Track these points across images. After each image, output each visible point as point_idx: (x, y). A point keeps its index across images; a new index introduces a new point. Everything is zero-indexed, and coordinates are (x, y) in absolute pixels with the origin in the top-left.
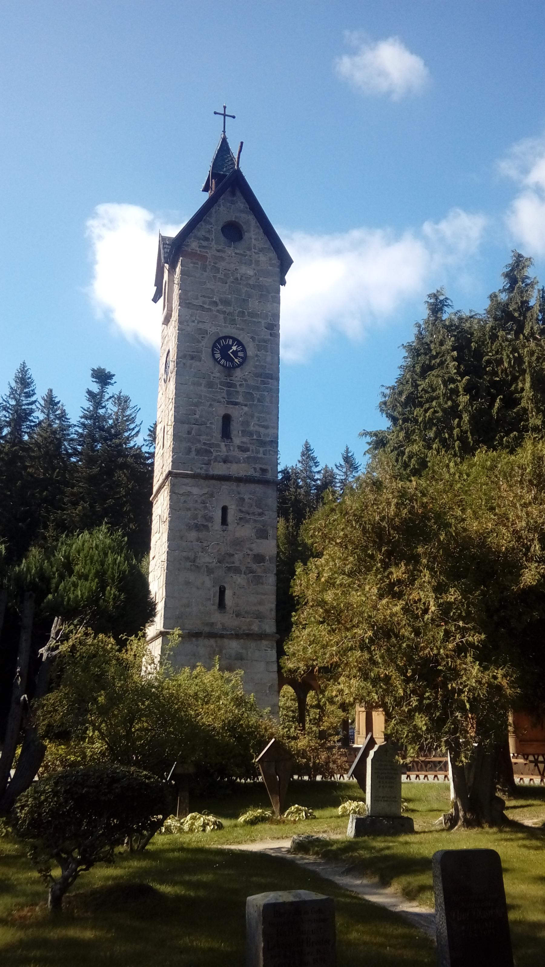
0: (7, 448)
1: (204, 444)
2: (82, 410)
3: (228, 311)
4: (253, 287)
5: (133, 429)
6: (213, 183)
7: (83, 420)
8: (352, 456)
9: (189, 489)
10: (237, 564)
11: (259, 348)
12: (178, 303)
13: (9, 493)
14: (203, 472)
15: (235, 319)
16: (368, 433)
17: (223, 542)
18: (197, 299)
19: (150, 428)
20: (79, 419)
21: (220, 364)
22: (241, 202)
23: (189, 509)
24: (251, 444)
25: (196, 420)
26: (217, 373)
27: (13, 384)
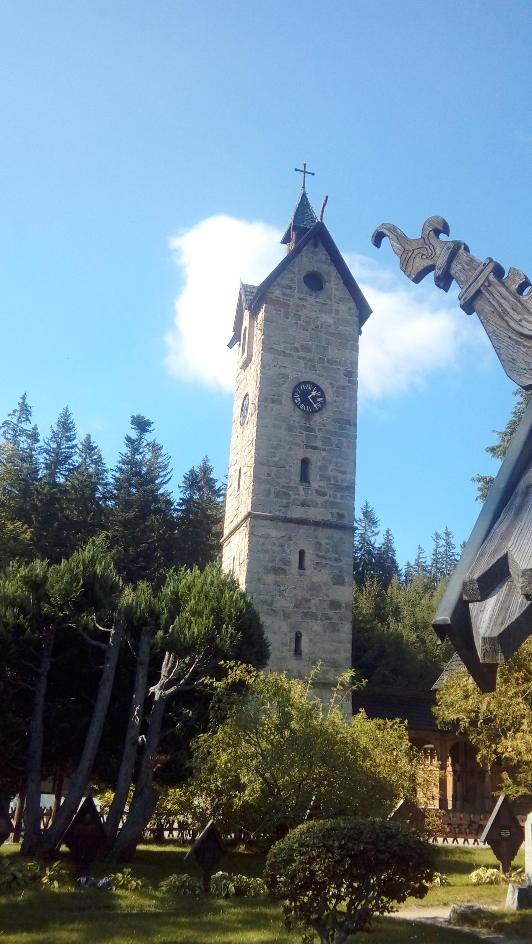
0: (46, 489)
1: (283, 487)
2: (120, 455)
3: (308, 357)
4: (333, 335)
5: (165, 476)
6: (293, 235)
7: (121, 465)
8: (371, 511)
9: (268, 531)
10: (313, 610)
11: (338, 394)
12: (261, 348)
13: (45, 534)
14: (281, 514)
15: (314, 366)
16: (482, 478)
17: (300, 587)
18: (279, 345)
19: (185, 475)
20: (117, 464)
21: (300, 408)
22: (323, 254)
23: (266, 552)
24: (328, 488)
25: (276, 462)
26: (297, 417)
27: (55, 428)
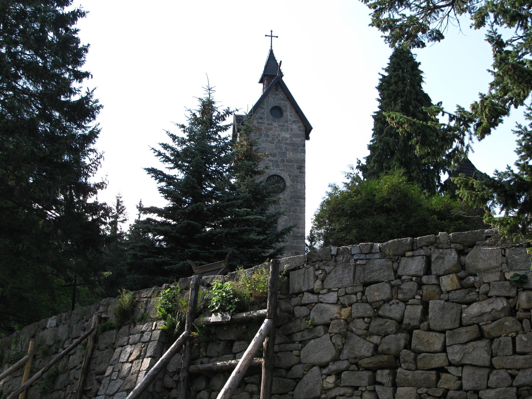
3: (274, 160)
11: (293, 181)
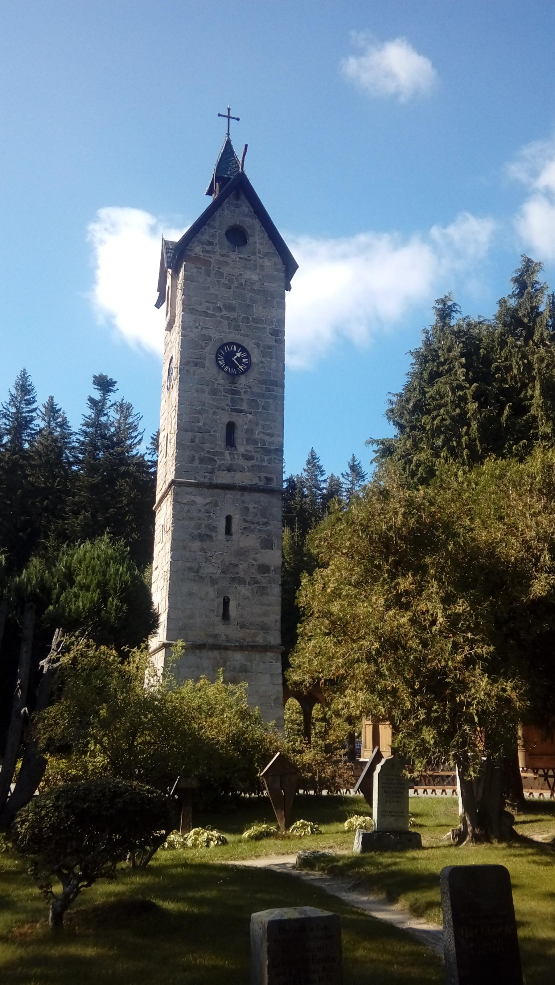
0: (7, 456)
1: (208, 452)
2: (83, 417)
3: (232, 317)
4: (258, 292)
5: (136, 437)
6: (217, 186)
7: (84, 428)
8: (358, 464)
9: (192, 498)
10: (241, 574)
11: (264, 355)
12: (181, 309)
13: (9, 502)
14: (206, 481)
15: (239, 325)
16: (375, 441)
17: (227, 553)
18: (201, 305)
19: (153, 436)
20: (81, 427)
21: (225, 371)
22: (245, 206)
23: (192, 519)
24: (255, 452)
25: (200, 428)
26: (221, 380)
27: (14, 392)
